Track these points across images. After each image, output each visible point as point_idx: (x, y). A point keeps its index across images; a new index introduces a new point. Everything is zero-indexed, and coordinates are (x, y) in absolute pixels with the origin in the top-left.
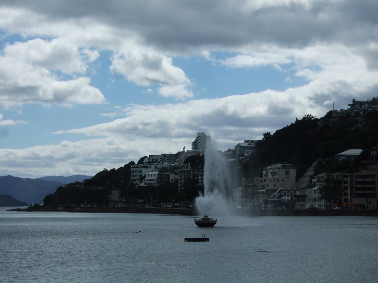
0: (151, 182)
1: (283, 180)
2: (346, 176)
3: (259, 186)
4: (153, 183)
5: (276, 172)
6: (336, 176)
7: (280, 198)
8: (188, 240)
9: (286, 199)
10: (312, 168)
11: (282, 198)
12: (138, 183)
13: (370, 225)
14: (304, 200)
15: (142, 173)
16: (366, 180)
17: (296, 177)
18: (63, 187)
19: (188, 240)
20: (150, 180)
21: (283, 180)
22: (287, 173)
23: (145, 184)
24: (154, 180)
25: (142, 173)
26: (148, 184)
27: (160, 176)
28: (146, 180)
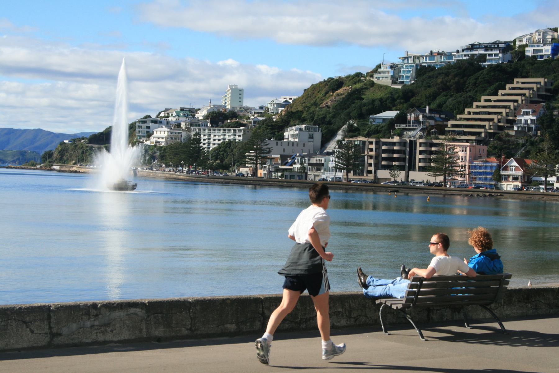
0: (159, 140)
1: (304, 144)
2: (371, 143)
3: (264, 150)
4: (162, 142)
5: (297, 134)
6: (359, 141)
7: (292, 166)
8: (480, 149)
9: (295, 168)
10: (340, 132)
11: (294, 166)
12: (143, 141)
13: (294, 271)
14: (318, 170)
15: (149, 129)
16: (432, 150)
17: (321, 142)
18: (66, 143)
19: (480, 149)
20: (159, 138)
21: (304, 144)
22: (311, 137)
23: (152, 142)
24: (162, 138)
25: (149, 129)
26: (156, 142)
27: (171, 134)
28: (154, 137)
